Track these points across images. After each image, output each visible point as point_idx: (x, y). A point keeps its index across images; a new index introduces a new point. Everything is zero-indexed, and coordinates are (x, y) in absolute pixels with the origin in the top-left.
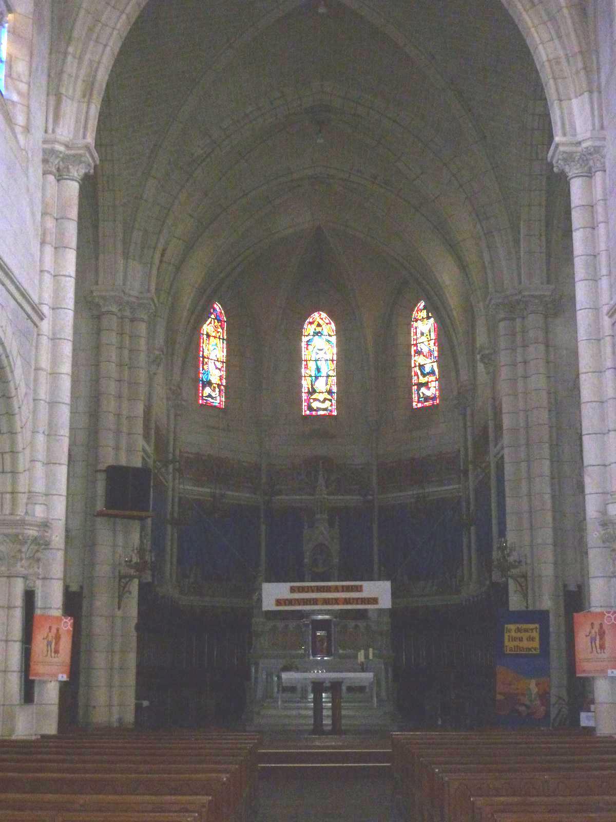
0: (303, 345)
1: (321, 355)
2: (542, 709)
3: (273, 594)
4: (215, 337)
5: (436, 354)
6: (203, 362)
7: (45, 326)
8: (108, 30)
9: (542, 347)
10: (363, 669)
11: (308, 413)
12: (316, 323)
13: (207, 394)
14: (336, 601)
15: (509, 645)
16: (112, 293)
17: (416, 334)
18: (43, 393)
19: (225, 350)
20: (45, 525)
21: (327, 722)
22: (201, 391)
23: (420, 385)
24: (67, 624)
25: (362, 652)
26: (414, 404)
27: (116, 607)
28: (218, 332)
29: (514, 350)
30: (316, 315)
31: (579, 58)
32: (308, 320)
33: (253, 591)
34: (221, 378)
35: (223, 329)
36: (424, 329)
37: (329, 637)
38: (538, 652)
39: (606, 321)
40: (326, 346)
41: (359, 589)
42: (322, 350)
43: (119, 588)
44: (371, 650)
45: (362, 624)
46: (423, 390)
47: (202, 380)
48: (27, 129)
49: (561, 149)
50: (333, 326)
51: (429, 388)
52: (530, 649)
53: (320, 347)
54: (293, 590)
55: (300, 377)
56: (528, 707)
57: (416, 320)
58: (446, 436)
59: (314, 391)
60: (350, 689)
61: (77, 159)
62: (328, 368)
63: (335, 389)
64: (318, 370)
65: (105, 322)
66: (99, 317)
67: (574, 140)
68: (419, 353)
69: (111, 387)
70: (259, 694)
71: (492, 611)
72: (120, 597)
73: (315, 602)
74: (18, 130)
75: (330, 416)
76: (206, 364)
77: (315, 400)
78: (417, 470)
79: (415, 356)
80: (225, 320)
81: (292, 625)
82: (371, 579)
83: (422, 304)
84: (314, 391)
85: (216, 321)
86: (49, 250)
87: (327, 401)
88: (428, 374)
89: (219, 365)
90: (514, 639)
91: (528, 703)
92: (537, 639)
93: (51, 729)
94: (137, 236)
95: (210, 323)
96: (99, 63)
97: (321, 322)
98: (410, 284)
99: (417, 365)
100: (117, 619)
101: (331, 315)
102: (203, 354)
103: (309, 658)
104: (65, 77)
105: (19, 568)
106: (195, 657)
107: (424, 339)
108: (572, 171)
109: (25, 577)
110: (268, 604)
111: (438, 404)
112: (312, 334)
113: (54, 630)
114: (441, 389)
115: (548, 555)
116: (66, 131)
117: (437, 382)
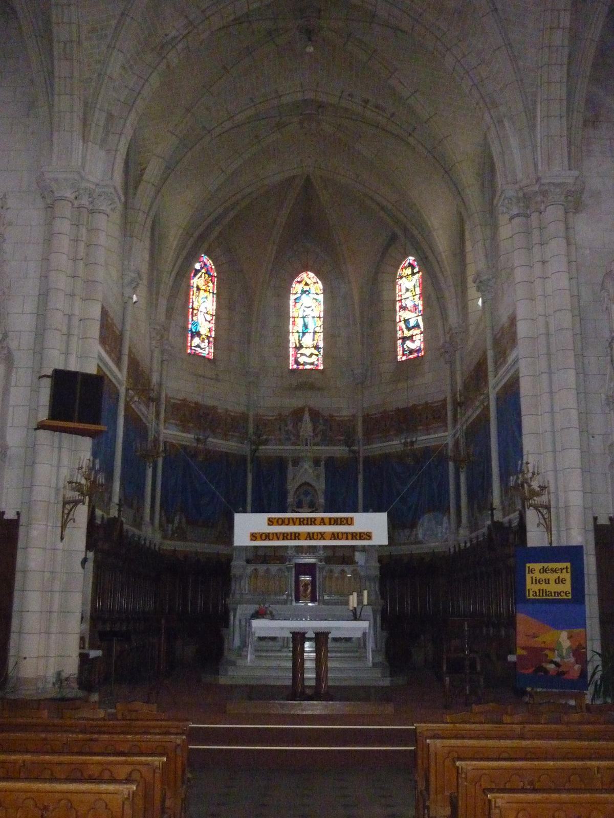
0: (292, 302)
1: (308, 311)
2: (577, 667)
3: (248, 527)
4: (205, 291)
5: (421, 308)
6: (192, 312)
9: (563, 242)
11: (295, 366)
12: (304, 283)
13: (196, 345)
14: (322, 536)
15: (532, 588)
17: (400, 291)
19: (215, 303)
22: (189, 341)
23: (404, 339)
25: (355, 594)
26: (399, 357)
27: (59, 538)
28: (209, 286)
29: (529, 249)
30: (304, 275)
32: (296, 280)
35: (213, 284)
36: (408, 287)
37: (313, 582)
38: (570, 597)
40: (313, 304)
41: (349, 522)
42: (309, 307)
43: (63, 517)
46: (408, 343)
47: (191, 330)
51: (413, 341)
52: (559, 594)
53: (307, 304)
54: (271, 522)
55: (288, 333)
56: (557, 665)
57: (401, 277)
58: (433, 387)
59: (301, 347)
62: (316, 325)
63: (321, 345)
64: (305, 326)
68: (404, 308)
69: (61, 281)
70: (237, 642)
72: (64, 526)
73: (297, 536)
76: (196, 315)
77: (302, 354)
78: (408, 419)
79: (399, 311)
80: (215, 274)
81: (274, 568)
84: (301, 347)
85: (206, 275)
87: (314, 356)
88: (414, 327)
89: (209, 318)
91: (558, 659)
94: (99, 117)
95: (201, 277)
97: (309, 282)
98: (399, 236)
99: (402, 319)
101: (317, 274)
102: (192, 306)
103: (291, 604)
107: (409, 294)
111: (422, 356)
112: (300, 292)
114: (425, 341)
115: (575, 481)
117: (422, 335)
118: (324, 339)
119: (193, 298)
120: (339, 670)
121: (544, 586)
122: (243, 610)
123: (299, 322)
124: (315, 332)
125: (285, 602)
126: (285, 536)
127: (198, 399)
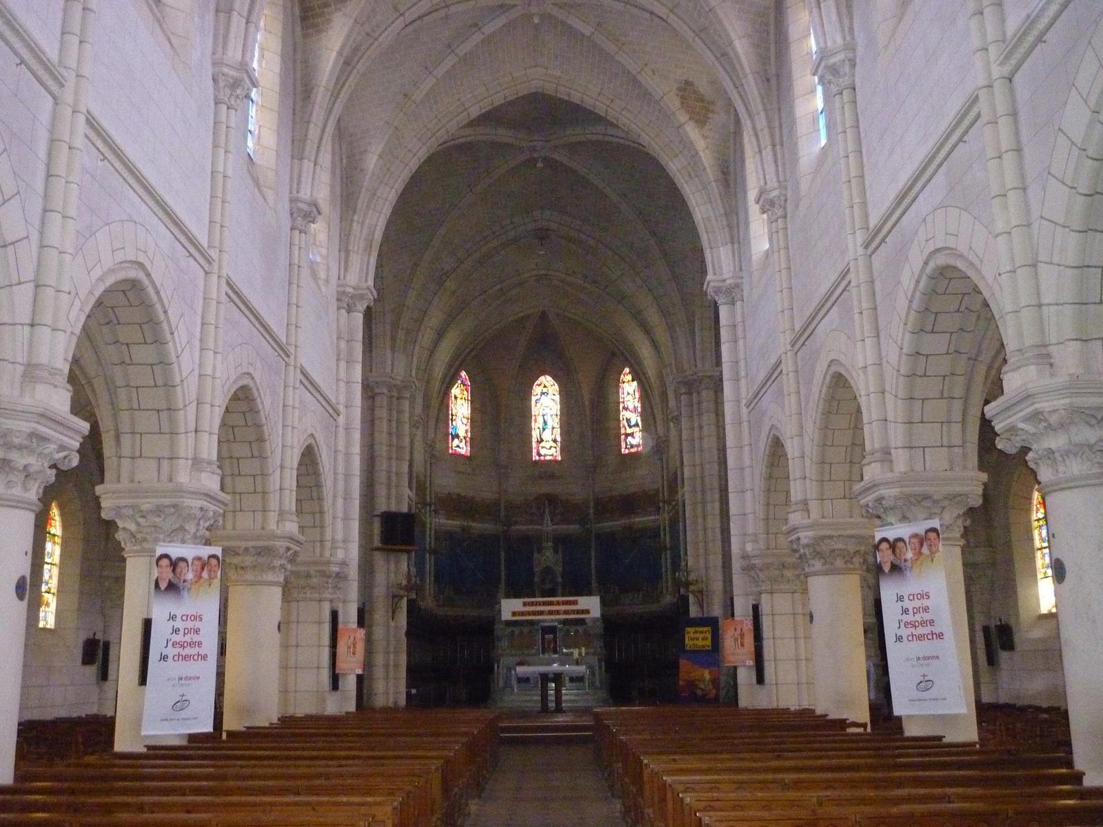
3: (510, 608)
5: (639, 410)
7: (341, 420)
8: (381, 201)
10: (577, 663)
11: (537, 458)
14: (558, 612)
15: (688, 643)
16: (384, 379)
18: (341, 469)
20: (344, 564)
21: (552, 705)
23: (627, 435)
24: (361, 633)
31: (724, 219)
33: (493, 603)
34: (466, 431)
36: (629, 392)
39: (744, 410)
40: (552, 404)
41: (575, 603)
44: (583, 649)
45: (581, 629)
48: (327, 281)
49: (712, 284)
50: (556, 387)
51: (633, 437)
53: (546, 403)
54: (525, 604)
55: (531, 429)
58: (645, 479)
60: (572, 680)
61: (362, 297)
62: (554, 422)
63: (559, 439)
64: (545, 423)
65: (378, 399)
66: (373, 398)
67: (720, 278)
68: (626, 409)
70: (501, 684)
71: (677, 619)
72: (394, 612)
73: (541, 613)
74: (321, 282)
75: (556, 461)
78: (629, 504)
81: (526, 630)
82: (582, 595)
83: (627, 370)
86: (343, 364)
89: (465, 421)
90: (692, 639)
92: (710, 640)
93: (352, 707)
94: (401, 335)
96: (376, 225)
98: (616, 356)
100: (393, 629)
104: (352, 239)
105: (327, 595)
106: (450, 658)
107: (630, 398)
108: (721, 300)
109: (331, 601)
110: (506, 615)
113: (352, 638)
116: (353, 278)
118: (561, 434)
119: (452, 406)
120: (571, 701)
121: (696, 642)
122: (505, 661)
123: (540, 420)
124: (553, 428)
125: (535, 655)
126: (534, 613)
127: (458, 491)
